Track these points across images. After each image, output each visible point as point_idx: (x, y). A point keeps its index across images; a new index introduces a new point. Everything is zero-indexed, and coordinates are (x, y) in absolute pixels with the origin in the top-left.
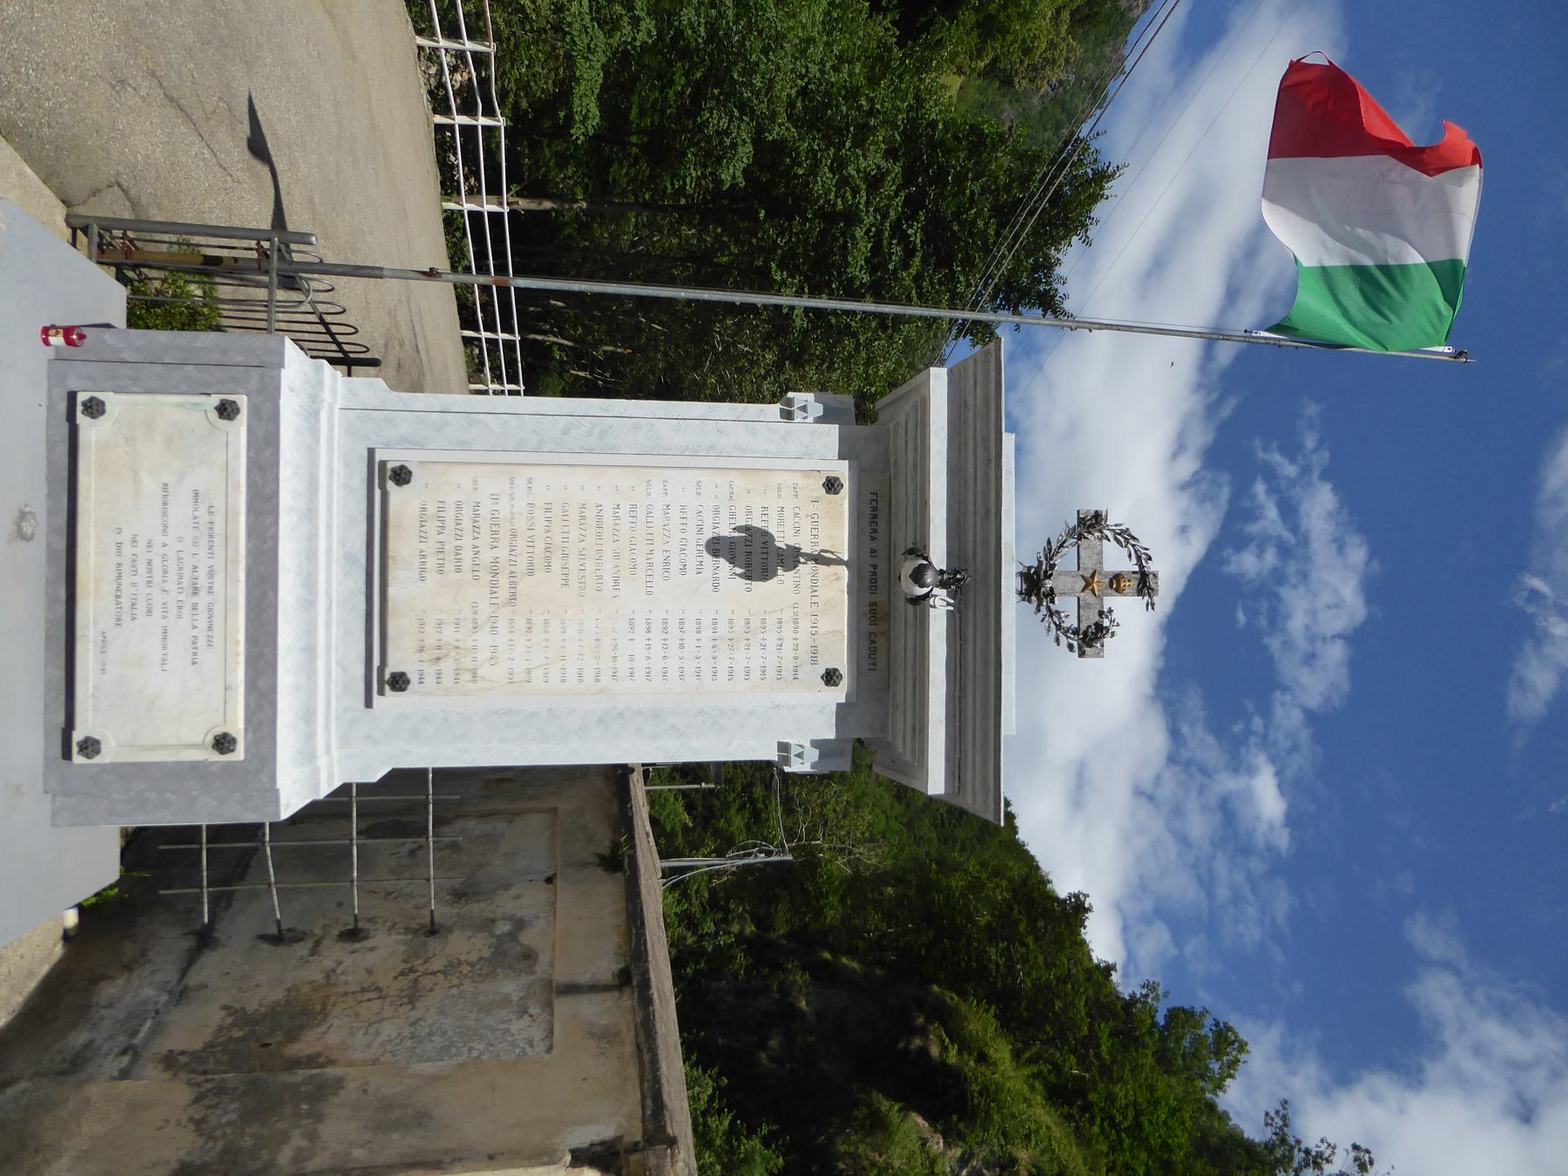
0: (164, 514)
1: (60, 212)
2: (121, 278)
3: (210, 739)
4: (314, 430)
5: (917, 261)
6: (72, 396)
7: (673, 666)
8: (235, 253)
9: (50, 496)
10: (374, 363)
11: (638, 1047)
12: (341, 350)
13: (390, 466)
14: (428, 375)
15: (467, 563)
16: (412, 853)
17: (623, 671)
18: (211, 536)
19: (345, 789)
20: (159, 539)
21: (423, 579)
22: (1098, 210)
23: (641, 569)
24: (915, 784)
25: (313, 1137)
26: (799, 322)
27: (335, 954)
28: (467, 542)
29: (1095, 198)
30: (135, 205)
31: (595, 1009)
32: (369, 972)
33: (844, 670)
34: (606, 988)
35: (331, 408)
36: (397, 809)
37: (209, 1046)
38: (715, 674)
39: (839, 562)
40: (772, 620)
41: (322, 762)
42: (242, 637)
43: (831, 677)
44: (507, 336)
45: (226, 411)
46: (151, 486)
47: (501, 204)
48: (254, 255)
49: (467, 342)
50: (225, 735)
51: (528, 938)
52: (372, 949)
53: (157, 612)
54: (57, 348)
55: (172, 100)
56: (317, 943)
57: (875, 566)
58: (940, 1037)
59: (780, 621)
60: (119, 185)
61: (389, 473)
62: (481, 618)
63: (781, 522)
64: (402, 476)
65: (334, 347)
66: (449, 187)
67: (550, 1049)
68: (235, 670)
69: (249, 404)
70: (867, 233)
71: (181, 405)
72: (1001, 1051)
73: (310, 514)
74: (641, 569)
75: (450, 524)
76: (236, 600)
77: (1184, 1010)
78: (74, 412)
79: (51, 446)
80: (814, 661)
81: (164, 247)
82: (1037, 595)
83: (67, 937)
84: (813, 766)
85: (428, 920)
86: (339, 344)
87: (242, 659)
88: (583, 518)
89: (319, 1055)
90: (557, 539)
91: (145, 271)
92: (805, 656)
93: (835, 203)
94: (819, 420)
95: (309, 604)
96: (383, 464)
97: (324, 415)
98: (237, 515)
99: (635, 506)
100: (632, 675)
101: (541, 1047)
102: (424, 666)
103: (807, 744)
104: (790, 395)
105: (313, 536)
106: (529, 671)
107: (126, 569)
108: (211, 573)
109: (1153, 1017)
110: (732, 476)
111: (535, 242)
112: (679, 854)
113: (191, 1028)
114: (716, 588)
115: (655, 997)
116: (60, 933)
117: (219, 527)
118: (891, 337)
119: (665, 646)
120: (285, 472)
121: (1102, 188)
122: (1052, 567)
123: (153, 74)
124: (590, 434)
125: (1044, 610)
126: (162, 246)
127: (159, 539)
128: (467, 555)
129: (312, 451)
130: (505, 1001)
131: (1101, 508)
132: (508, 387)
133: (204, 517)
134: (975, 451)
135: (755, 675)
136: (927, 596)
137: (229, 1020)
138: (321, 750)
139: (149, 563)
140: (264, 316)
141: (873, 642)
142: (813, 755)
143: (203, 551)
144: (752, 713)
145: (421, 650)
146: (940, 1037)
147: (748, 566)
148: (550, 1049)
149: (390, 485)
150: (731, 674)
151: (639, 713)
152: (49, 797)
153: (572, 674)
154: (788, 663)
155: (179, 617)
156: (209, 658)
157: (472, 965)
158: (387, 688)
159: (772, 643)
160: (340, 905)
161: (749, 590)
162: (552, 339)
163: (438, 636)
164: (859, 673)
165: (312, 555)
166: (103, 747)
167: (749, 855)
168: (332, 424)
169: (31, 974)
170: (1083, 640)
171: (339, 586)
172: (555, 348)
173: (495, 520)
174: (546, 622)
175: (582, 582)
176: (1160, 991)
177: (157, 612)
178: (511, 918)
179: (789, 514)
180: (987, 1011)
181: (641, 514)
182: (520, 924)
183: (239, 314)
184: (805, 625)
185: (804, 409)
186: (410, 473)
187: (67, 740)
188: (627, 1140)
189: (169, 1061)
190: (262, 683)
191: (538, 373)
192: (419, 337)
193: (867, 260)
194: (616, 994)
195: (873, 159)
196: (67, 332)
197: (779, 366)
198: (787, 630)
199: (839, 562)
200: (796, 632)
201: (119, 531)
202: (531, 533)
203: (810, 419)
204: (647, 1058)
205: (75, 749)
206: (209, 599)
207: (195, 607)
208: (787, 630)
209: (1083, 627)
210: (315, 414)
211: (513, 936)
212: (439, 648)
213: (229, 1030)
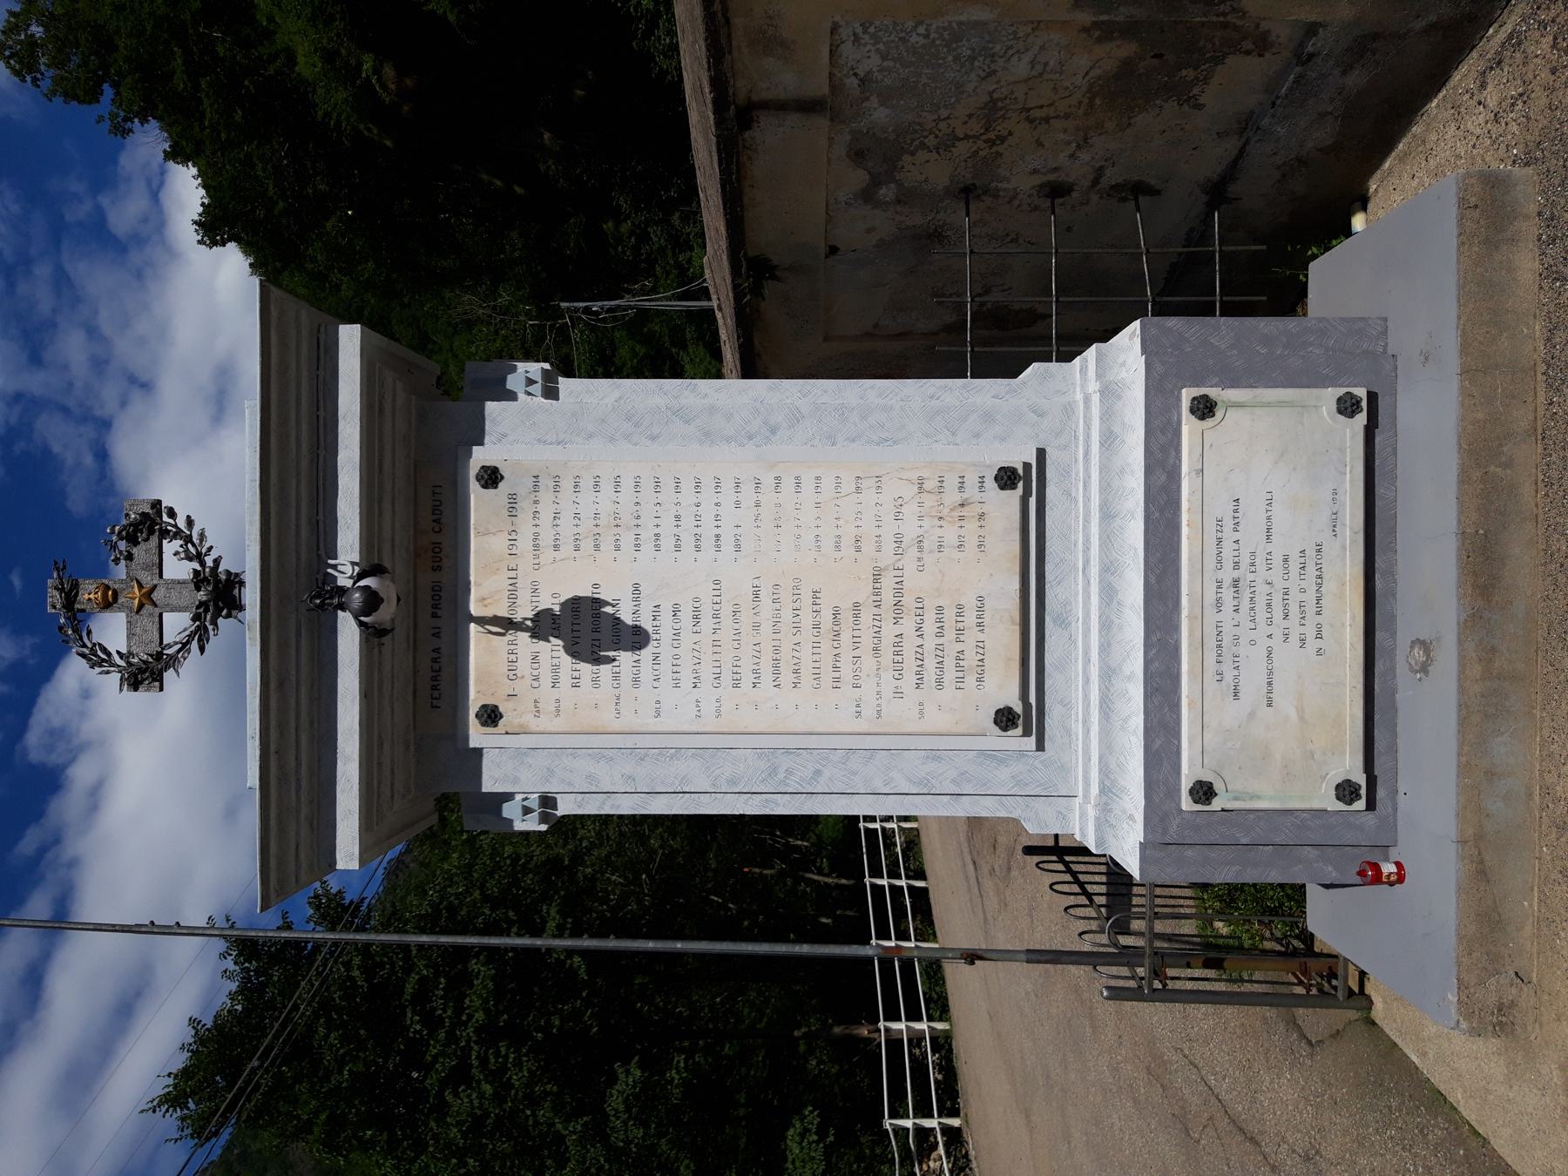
0: (1271, 672)
1: (1379, 1011)
2: (1308, 938)
3: (1219, 413)
4: (1105, 772)
5: (409, 989)
6: (1371, 805)
8: (1189, 972)
9: (1393, 692)
10: (1030, 850)
11: (728, 21)
12: (1066, 864)
13: (1019, 730)
14: (962, 837)
15: (930, 617)
16: (987, 291)
18: (1219, 646)
19: (1067, 357)
21: (980, 599)
22: (180, 1061)
23: (726, 610)
24: (377, 338)
26: (552, 912)
27: (1077, 170)
28: (930, 643)
29: (185, 1074)
30: (1293, 1023)
31: (783, 80)
32: (1039, 144)
33: (474, 487)
34: (765, 105)
35: (1086, 796)
36: (1004, 335)
37: (1218, 60)
39: (481, 621)
40: (567, 549)
41: (1093, 386)
42: (1185, 530)
43: (491, 477)
44: (879, 882)
45: (1204, 792)
46: (1286, 704)
47: (887, 1030)
48: (1171, 972)
49: (921, 875)
50: (1202, 418)
51: (858, 178)
52: (1035, 171)
54: (1387, 860)
55: (1252, 1140)
56: (1096, 182)
57: (435, 616)
58: (384, 87)
59: (556, 547)
60: (1309, 1043)
61: (1020, 722)
62: (913, 553)
63: (556, 668)
64: (1005, 719)
65: (1075, 867)
66: (943, 1044)
67: (834, 29)
68: (1192, 493)
70: (470, 1017)
71: (1253, 797)
72: (307, 66)
73: (1109, 674)
75: (949, 663)
76: (1191, 574)
77: (75, 97)
78: (1367, 789)
79: (1393, 749)
80: (513, 498)
81: (1257, 976)
82: (218, 581)
83: (1363, 203)
84: (514, 369)
85: (972, 207)
86: (1069, 871)
89: (1099, 40)
90: (826, 645)
91: (1278, 948)
92: (525, 505)
93: (508, 1049)
94: (508, 797)
95: (1109, 569)
97: (1095, 790)
98: (1190, 672)
101: (845, 33)
102: (978, 496)
103: (521, 396)
104: (544, 827)
105: (1105, 648)
106: (858, 490)
107: (1311, 608)
108: (1219, 603)
109: (117, 94)
110: (617, 725)
111: (851, 991)
112: (689, 314)
113: (1237, 82)
116: (1370, 206)
117: (1211, 658)
118: (442, 898)
119: (698, 518)
120: (1138, 721)
121: (175, 1086)
122: (196, 618)
123: (1273, 1168)
124: (789, 772)
125: (209, 561)
126: (1259, 977)
128: (930, 627)
129: (1108, 746)
131: (128, 694)
132: (877, 826)
133: (1227, 668)
134: (298, 764)
136: (361, 576)
137: (1195, 91)
138: (1096, 398)
140: (1158, 901)
141: (437, 521)
142: (514, 382)
143: (1228, 630)
146: (384, 87)
147: (598, 615)
148: (834, 29)
149: (1018, 708)
150: (617, 484)
151: (728, 440)
152: (1390, 352)
154: (546, 497)
156: (1223, 508)
157: (923, 146)
158: (1021, 472)
159: (566, 521)
160: (1069, 229)
162: (829, 880)
164: (455, 483)
165: (1106, 626)
166: (1334, 406)
167: (610, 310)
168: (1084, 777)
169: (1401, 160)
170: (154, 523)
171: (1075, 592)
172: (826, 871)
173: (898, 667)
174: (838, 547)
175: (797, 595)
176: (107, 125)
179: (546, 680)
180: (327, 115)
181: (727, 678)
182: (867, 195)
183: (1172, 902)
184: (525, 544)
185: (527, 811)
187: (1371, 412)
189: (1263, 44)
191: (842, 841)
192: (973, 881)
193: (471, 986)
194: (755, 98)
195: (462, 1103)
196: (1377, 879)
197: (577, 858)
199: (481, 621)
200: (536, 535)
201: (1319, 652)
202: (856, 653)
203: (519, 797)
205: (1364, 404)
206: (1220, 575)
207: (1236, 565)
208: (547, 539)
209: (154, 540)
210: (1104, 790)
211: (876, 181)
212: (962, 518)
213: (1197, 78)
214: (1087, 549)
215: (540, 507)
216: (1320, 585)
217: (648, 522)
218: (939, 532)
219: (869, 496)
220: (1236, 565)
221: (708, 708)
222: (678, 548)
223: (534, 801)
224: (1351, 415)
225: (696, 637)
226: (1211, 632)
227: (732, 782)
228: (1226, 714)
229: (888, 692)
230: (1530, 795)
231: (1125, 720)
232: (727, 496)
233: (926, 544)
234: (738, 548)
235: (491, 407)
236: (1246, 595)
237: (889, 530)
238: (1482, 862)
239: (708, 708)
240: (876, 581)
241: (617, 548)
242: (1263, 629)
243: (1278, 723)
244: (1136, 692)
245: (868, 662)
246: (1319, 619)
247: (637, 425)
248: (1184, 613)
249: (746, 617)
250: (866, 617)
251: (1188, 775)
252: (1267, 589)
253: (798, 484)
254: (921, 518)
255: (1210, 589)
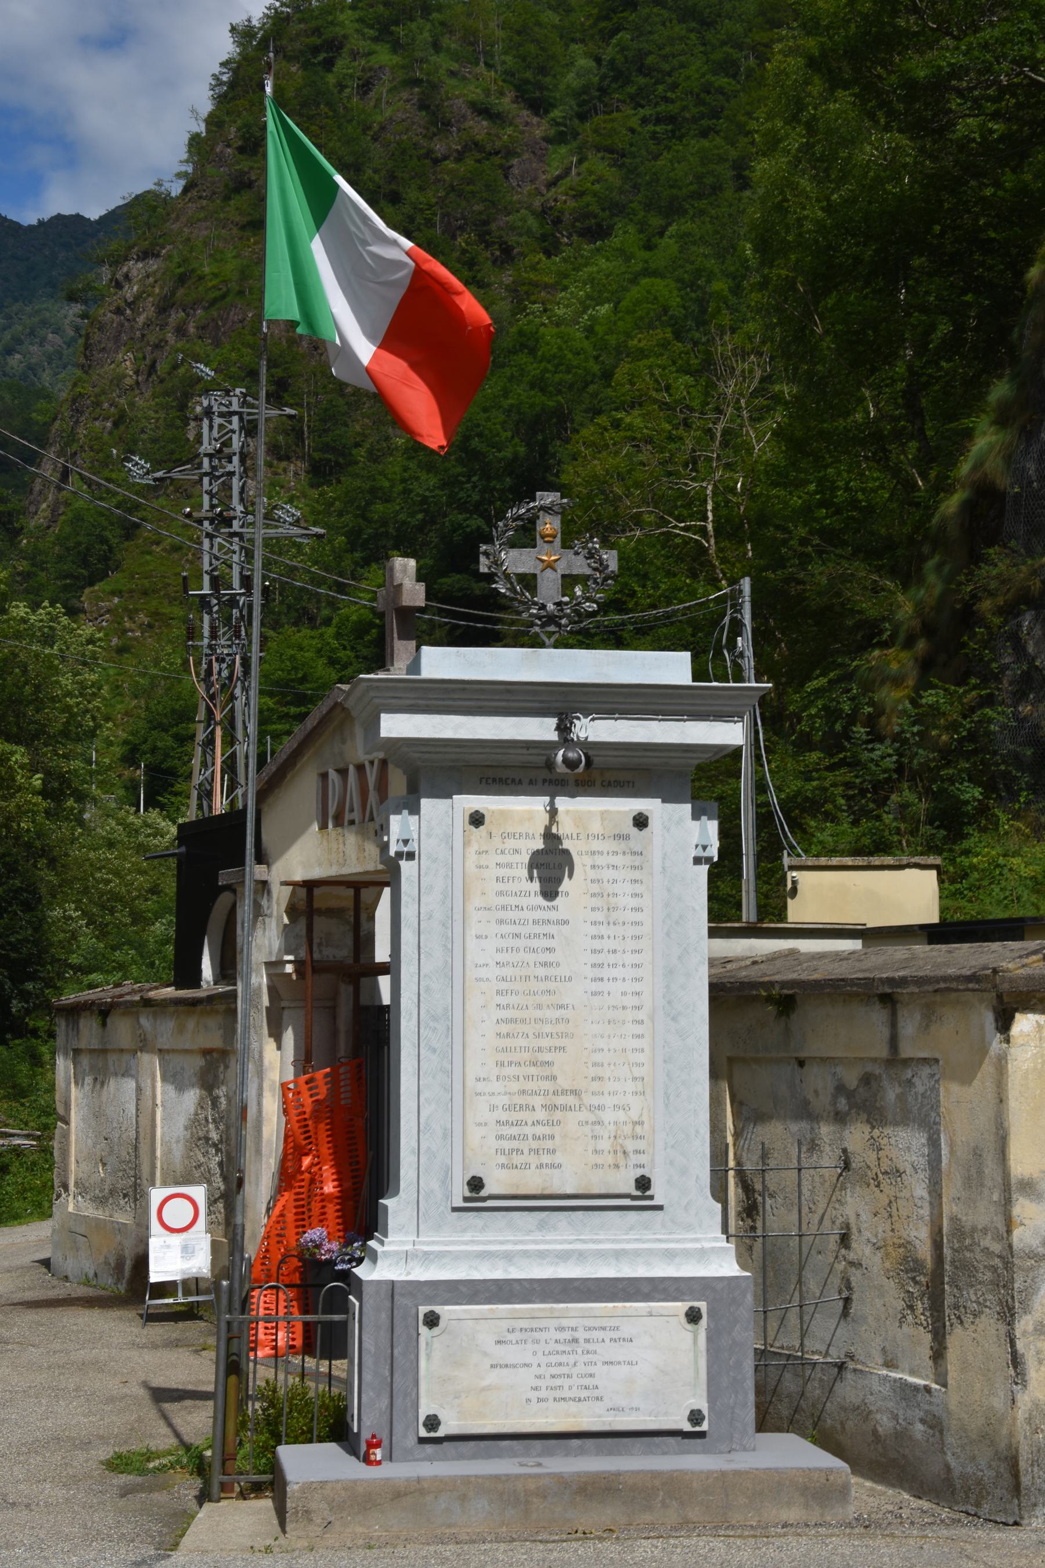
0: (515, 1366)
3: (689, 1327)
6: (422, 1441)
7: (630, 959)
13: (468, 1194)
17: (635, 1001)
20: (535, 1370)
21: (560, 1166)
23: (551, 985)
25: (985, 1231)
27: (861, 1249)
28: (529, 1130)
31: (909, 1025)
38: (637, 923)
41: (707, 1245)
45: (432, 1321)
46: (493, 1377)
51: (852, 1079)
53: (591, 1369)
59: (593, 867)
61: (474, 1195)
62: (592, 1118)
64: (476, 1184)
68: (636, 1309)
69: (419, 1306)
71: (429, 1357)
73: (508, 1257)
74: (551, 985)
75: (515, 1144)
78: (435, 1439)
80: (626, 837)
87: (628, 1304)
88: (508, 1035)
90: (526, 1056)
92: (622, 845)
96: (466, 1199)
98: (515, 1310)
99: (498, 992)
100: (638, 994)
102: (631, 1164)
104: (392, 853)
105: (526, 1254)
106: (635, 1079)
107: (558, 1394)
108: (561, 1329)
110: (470, 908)
114: (566, 922)
115: (901, 973)
119: (615, 966)
120: (476, 1276)
127: (535, 1370)
128: (540, 1130)
130: (901, 1098)
134: (454, 699)
135: (638, 888)
138: (698, 1246)
139: (553, 1376)
143: (542, 1336)
144: (669, 890)
145: (617, 1166)
148: (937, 1061)
149: (484, 1193)
151: (668, 987)
153: (636, 1043)
154: (628, 860)
155: (595, 1352)
156: (626, 1331)
158: (648, 1193)
159: (610, 874)
161: (567, 894)
163: (606, 1153)
165: (542, 1255)
166: (695, 1408)
168: (431, 1241)
173: (511, 1108)
174: (595, 1064)
177: (591, 1369)
178: (835, 1097)
179: (501, 859)
181: (504, 986)
182: (840, 1089)
186: (473, 1177)
187: (691, 1436)
188: (995, 1002)
190: (646, 1289)
194: (899, 1006)
198: (600, 860)
201: (528, 1400)
204: (942, 985)
205: (697, 1429)
207: (587, 1341)
208: (600, 860)
210: (426, 1254)
211: (850, 1095)
212: (615, 1152)
214: (594, 1241)
215: (620, 856)
216: (574, 1400)
217: (612, 930)
218: (606, 1136)
219: (630, 1086)
220: (587, 1341)
221: (483, 973)
222: (594, 951)
223: (413, 846)
224: (690, 1419)
225: (532, 964)
226: (542, 1324)
227: (428, 989)
228: (486, 1338)
229: (495, 1100)
230: (449, 1526)
231: (476, 1268)
232: (630, 987)
233: (597, 1127)
234: (594, 994)
235: (687, 808)
236: (567, 1348)
237: (608, 1101)
238: (406, 1495)
239: (483, 973)
240: (572, 1092)
241: (593, 909)
242: (544, 1360)
243: (479, 1376)
244: (498, 1274)
245: (515, 1086)
246: (551, 1400)
247: (677, 923)
248: (555, 1306)
249: (545, 999)
250: (546, 1085)
251: (445, 1311)
252: (572, 1362)
253: (638, 1036)
254: (615, 1123)
255: (572, 1323)
